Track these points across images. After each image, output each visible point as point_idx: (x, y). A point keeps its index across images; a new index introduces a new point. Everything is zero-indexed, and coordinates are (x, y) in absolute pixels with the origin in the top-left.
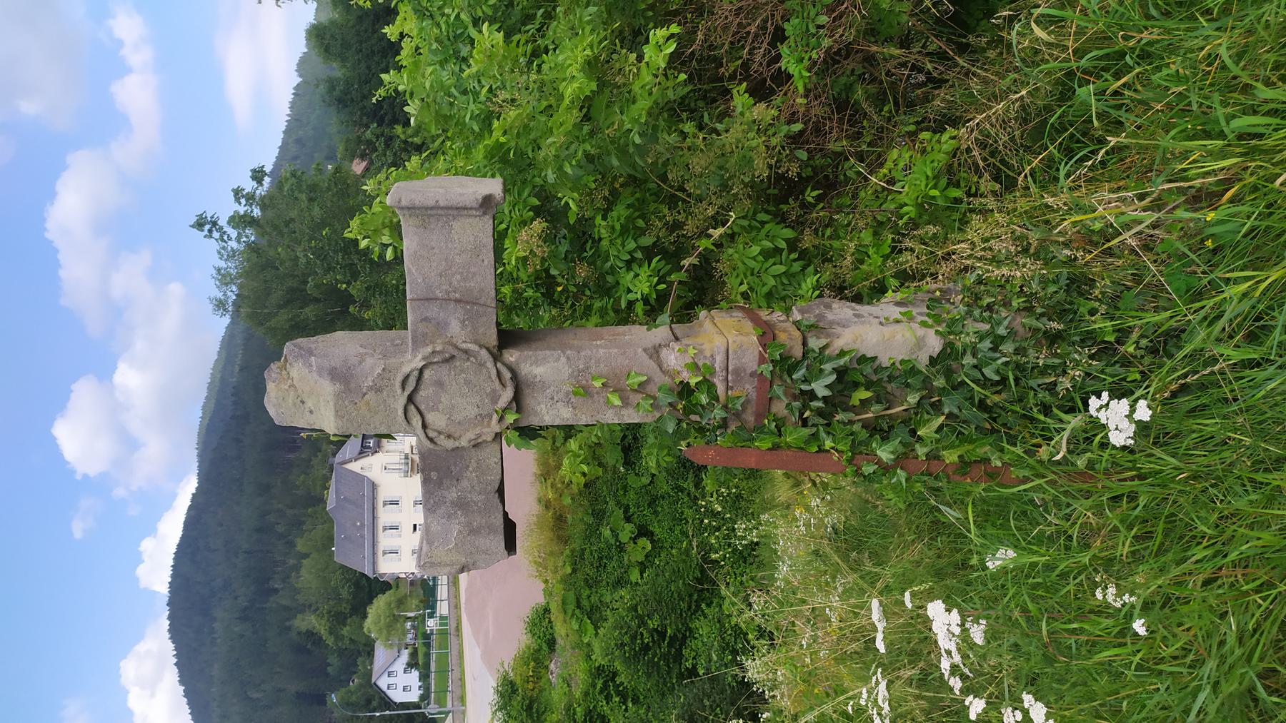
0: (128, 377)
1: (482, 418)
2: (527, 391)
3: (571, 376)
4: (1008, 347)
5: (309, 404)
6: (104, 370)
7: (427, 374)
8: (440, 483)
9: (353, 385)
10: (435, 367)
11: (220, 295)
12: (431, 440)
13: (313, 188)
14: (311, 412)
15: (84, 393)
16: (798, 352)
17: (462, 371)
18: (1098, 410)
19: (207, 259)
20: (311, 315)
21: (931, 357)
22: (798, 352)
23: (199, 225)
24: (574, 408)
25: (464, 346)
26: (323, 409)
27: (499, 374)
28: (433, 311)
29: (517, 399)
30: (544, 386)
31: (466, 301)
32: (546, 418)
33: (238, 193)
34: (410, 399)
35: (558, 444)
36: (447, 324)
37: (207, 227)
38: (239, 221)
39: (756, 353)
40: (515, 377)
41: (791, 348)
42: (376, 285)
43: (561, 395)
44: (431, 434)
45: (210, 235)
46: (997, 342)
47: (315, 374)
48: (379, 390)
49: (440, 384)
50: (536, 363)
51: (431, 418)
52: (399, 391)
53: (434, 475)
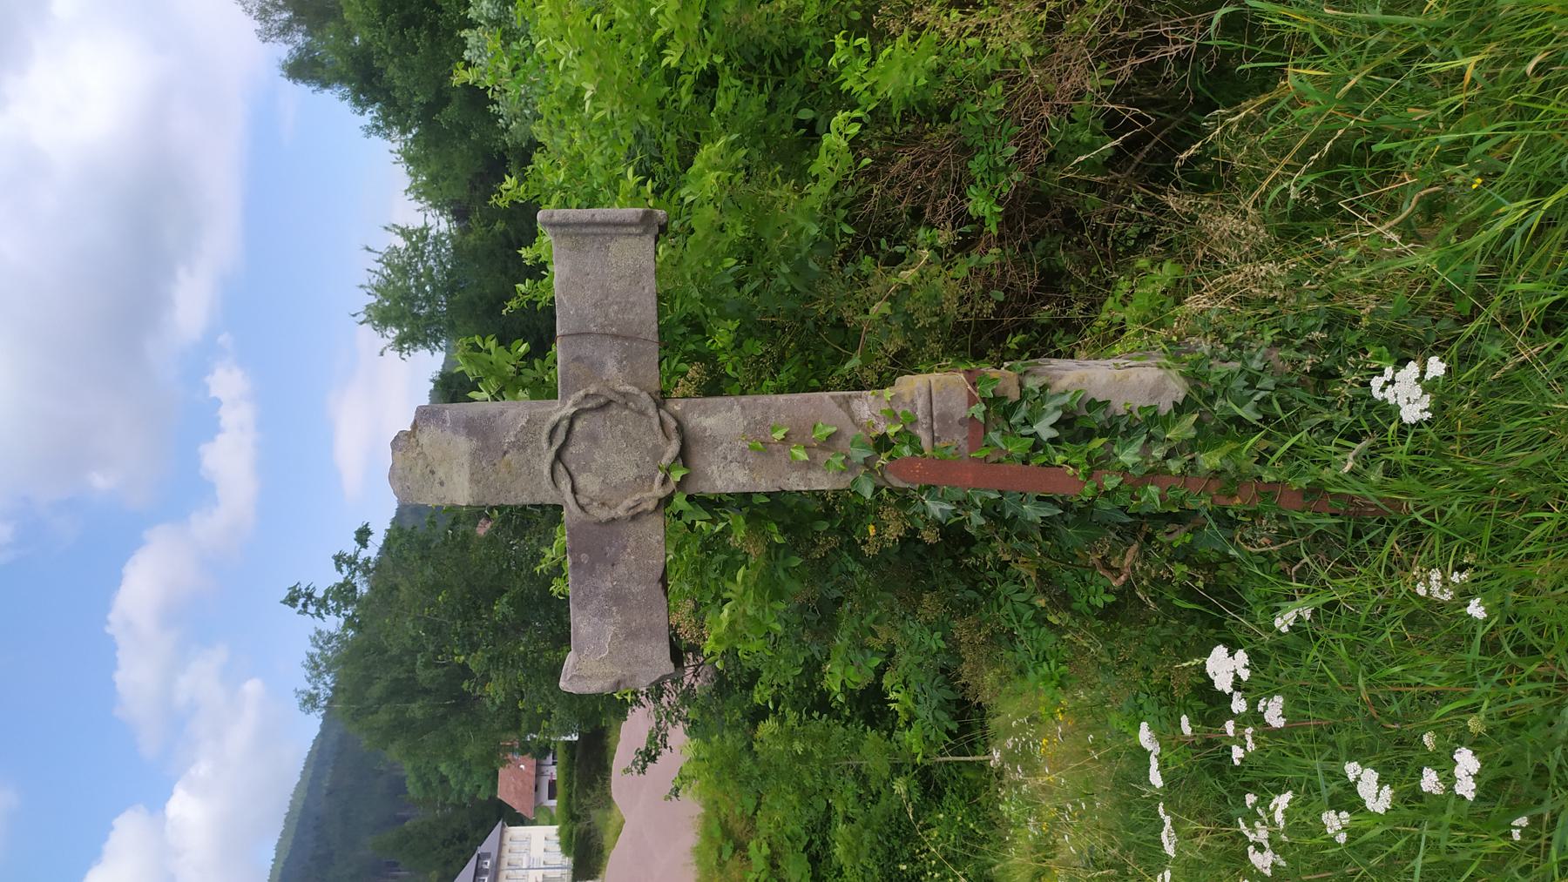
0: (188, 809)
1: (644, 481)
2: (694, 449)
3: (746, 429)
4: (1267, 382)
5: (440, 473)
6: (156, 800)
8: (591, 570)
9: (492, 441)
10: (587, 416)
11: (309, 687)
12: (582, 508)
13: (425, 545)
14: (442, 484)
15: (128, 830)
16: (1014, 395)
17: (619, 422)
18: (1383, 390)
19: (302, 636)
20: (419, 714)
21: (1175, 403)
22: (1014, 395)
23: (291, 600)
24: (751, 470)
25: (622, 389)
26: (455, 476)
27: (662, 423)
28: (587, 348)
29: (683, 456)
30: (715, 443)
31: (623, 337)
32: (719, 483)
33: (339, 560)
34: (559, 456)
35: (725, 857)
36: (603, 364)
37: (302, 600)
38: (344, 593)
39: (965, 394)
40: (680, 428)
41: (1006, 389)
42: (501, 655)
43: (736, 454)
44: (583, 501)
45: (304, 611)
46: (1252, 381)
47: (448, 432)
48: (523, 448)
49: (593, 438)
50: (704, 413)
51: (581, 481)
52: (545, 445)
53: (584, 558)
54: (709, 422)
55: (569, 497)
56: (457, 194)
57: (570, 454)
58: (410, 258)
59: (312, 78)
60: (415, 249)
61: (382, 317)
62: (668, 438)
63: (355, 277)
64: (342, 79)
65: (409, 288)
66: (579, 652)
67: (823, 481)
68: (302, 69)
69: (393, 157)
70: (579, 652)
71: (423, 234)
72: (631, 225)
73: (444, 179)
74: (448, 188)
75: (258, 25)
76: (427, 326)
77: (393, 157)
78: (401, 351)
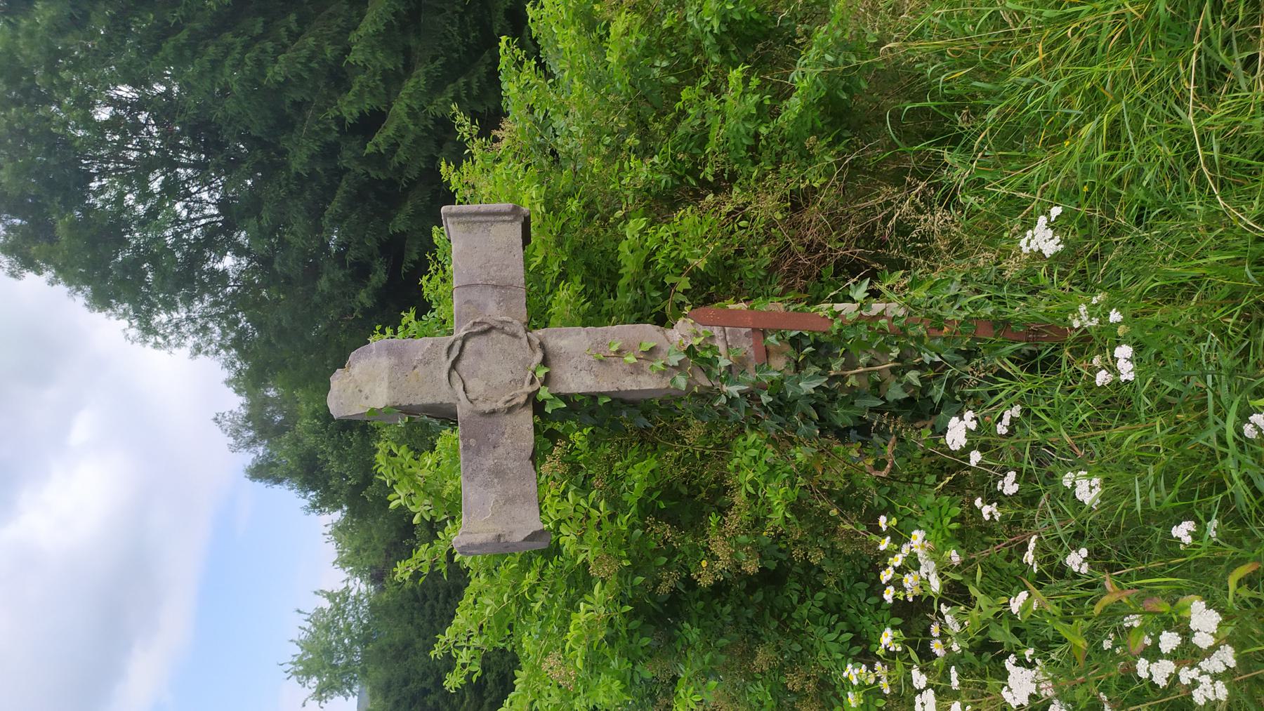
7: (468, 345)
8: (478, 451)
9: (405, 359)
17: (498, 342)
28: (474, 294)
29: (545, 362)
32: (572, 385)
34: (454, 366)
43: (584, 364)
49: (479, 353)
51: (470, 385)
52: (444, 358)
54: (563, 343)
55: (461, 394)
56: (374, 561)
57: (464, 363)
58: (334, 616)
59: (269, 477)
60: (338, 609)
61: (306, 670)
62: (534, 351)
63: (287, 633)
64: (291, 474)
65: (330, 643)
66: (468, 515)
67: (648, 382)
68: (261, 472)
69: (325, 538)
70: (468, 515)
71: (344, 595)
72: (505, 214)
73: (365, 550)
74: (368, 557)
75: (231, 440)
76: (342, 675)
77: (325, 538)
78: (320, 700)
